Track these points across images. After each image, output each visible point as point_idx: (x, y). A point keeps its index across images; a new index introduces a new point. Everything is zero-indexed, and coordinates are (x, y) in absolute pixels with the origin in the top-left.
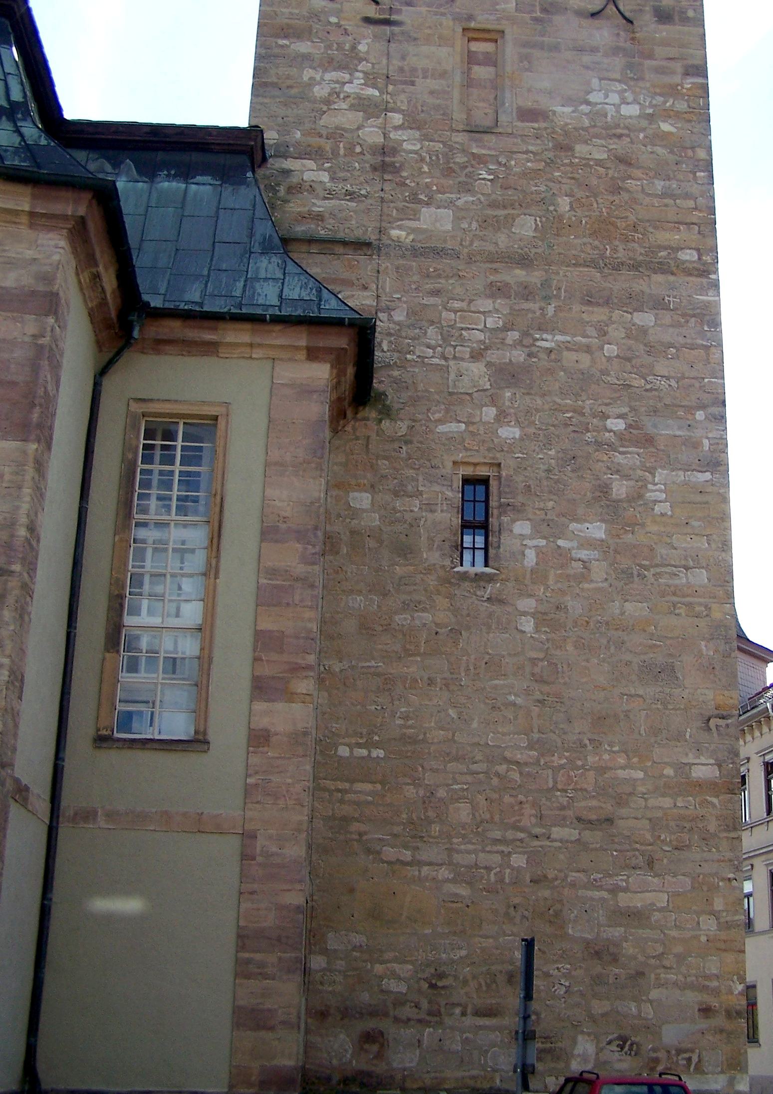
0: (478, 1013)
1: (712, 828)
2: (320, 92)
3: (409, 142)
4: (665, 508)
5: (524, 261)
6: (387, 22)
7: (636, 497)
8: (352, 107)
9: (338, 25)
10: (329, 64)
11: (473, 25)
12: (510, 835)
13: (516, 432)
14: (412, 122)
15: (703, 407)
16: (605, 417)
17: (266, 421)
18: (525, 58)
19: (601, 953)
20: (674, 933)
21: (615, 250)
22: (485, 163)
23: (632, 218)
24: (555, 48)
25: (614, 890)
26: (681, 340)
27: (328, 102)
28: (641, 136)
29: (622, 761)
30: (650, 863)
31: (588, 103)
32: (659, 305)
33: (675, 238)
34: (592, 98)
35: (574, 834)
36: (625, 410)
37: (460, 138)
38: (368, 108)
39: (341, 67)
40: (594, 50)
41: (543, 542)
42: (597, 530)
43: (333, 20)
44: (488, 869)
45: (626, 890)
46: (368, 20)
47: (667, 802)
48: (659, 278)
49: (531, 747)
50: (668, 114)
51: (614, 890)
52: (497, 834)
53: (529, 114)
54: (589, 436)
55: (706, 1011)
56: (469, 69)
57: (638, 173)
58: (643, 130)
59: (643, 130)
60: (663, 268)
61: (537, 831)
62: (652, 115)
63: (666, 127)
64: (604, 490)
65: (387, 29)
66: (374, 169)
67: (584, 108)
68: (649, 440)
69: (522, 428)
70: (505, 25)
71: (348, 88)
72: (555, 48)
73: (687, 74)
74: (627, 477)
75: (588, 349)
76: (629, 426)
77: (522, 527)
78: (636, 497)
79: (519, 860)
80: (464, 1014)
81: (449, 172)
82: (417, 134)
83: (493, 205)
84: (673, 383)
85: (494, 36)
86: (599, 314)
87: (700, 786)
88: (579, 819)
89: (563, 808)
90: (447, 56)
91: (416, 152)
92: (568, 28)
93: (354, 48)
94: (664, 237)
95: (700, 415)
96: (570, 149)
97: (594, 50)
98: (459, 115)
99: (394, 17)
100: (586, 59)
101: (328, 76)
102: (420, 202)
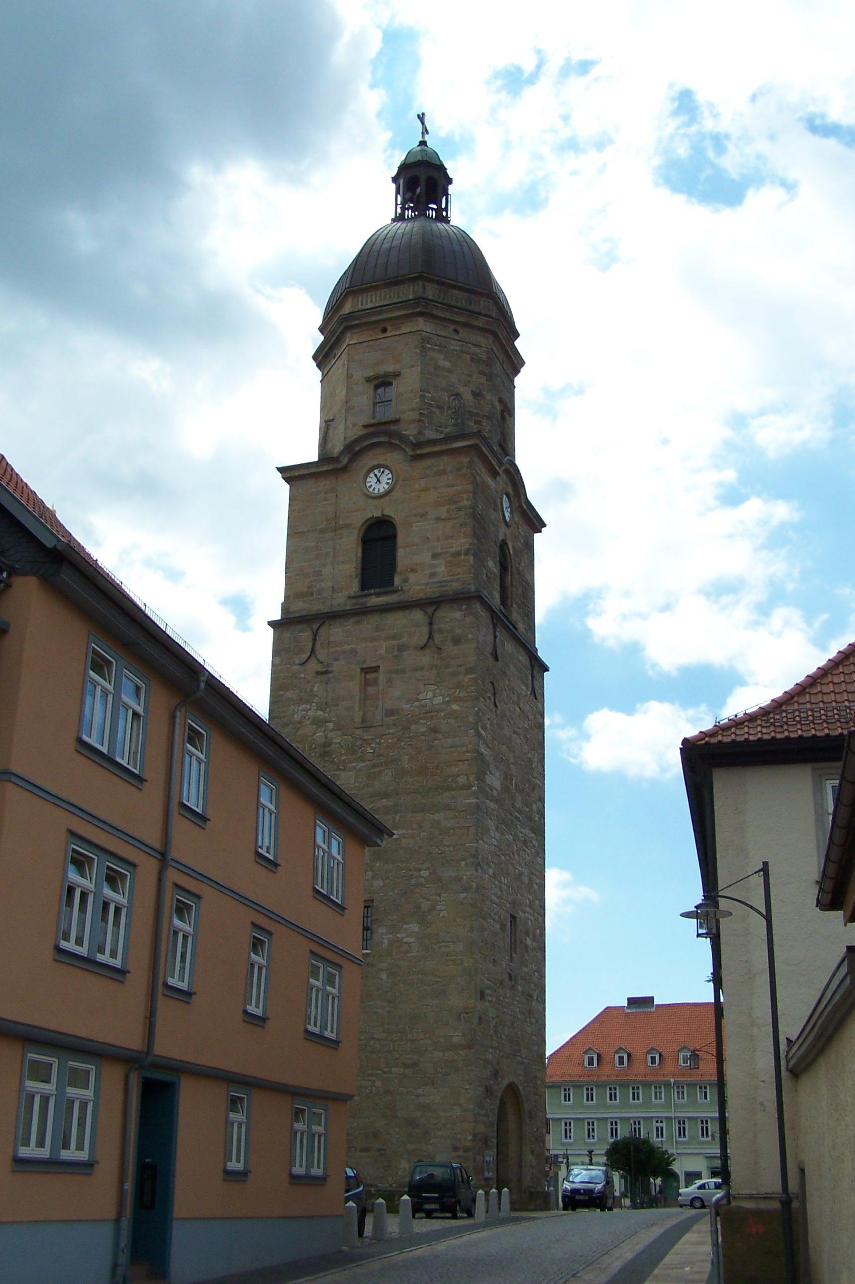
0: (361, 1151)
1: (460, 1065)
2: (297, 717)
3: (337, 738)
4: (444, 913)
5: (386, 795)
6: (326, 672)
7: (433, 908)
8: (312, 723)
9: (305, 678)
10: (301, 701)
11: (365, 666)
12: (375, 1071)
13: (381, 883)
14: (339, 728)
15: (464, 860)
16: (419, 870)
17: (427, 636)
18: (389, 680)
19: (411, 1123)
20: (442, 1114)
21: (427, 781)
22: (370, 744)
23: (437, 762)
24: (403, 671)
25: (418, 1096)
26: (456, 825)
27: (300, 723)
28: (443, 714)
29: (422, 1036)
30: (433, 1084)
31: (417, 700)
32: (447, 807)
33: (454, 770)
34: (420, 697)
35: (400, 1070)
36: (429, 865)
37: (358, 732)
38: (319, 723)
39: (307, 702)
40: (422, 669)
41: (391, 936)
42: (415, 927)
43: (302, 676)
44: (366, 1087)
45: (423, 1095)
46: (318, 673)
47: (441, 1054)
48: (447, 794)
49: (384, 1032)
50: (457, 700)
51: (418, 1096)
52: (370, 1072)
53: (390, 713)
54: (413, 881)
55: (456, 1149)
56: (365, 690)
57: (440, 736)
58: (444, 710)
59: (444, 710)
60: (450, 789)
61: (386, 1070)
62: (448, 702)
63: (455, 707)
64: (418, 907)
65: (326, 677)
66: (321, 755)
67: (417, 704)
68: (439, 879)
69: (383, 880)
70: (380, 663)
71: (310, 713)
72: (403, 671)
73: (466, 674)
74: (429, 900)
75: (413, 837)
76: (431, 874)
77: (382, 930)
78: (433, 908)
79: (378, 1083)
80: (356, 1151)
81: (354, 752)
82: (339, 733)
83: (374, 766)
84: (451, 849)
85: (376, 669)
86: (419, 816)
87: (455, 1047)
88: (403, 1064)
89: (396, 1059)
90: (354, 686)
91: (339, 743)
92: (410, 658)
93: (312, 690)
94: (454, 770)
95: (463, 864)
96: (408, 728)
97: (422, 669)
98: (358, 719)
99: (330, 669)
100: (418, 674)
101: (301, 708)
102: (340, 770)
